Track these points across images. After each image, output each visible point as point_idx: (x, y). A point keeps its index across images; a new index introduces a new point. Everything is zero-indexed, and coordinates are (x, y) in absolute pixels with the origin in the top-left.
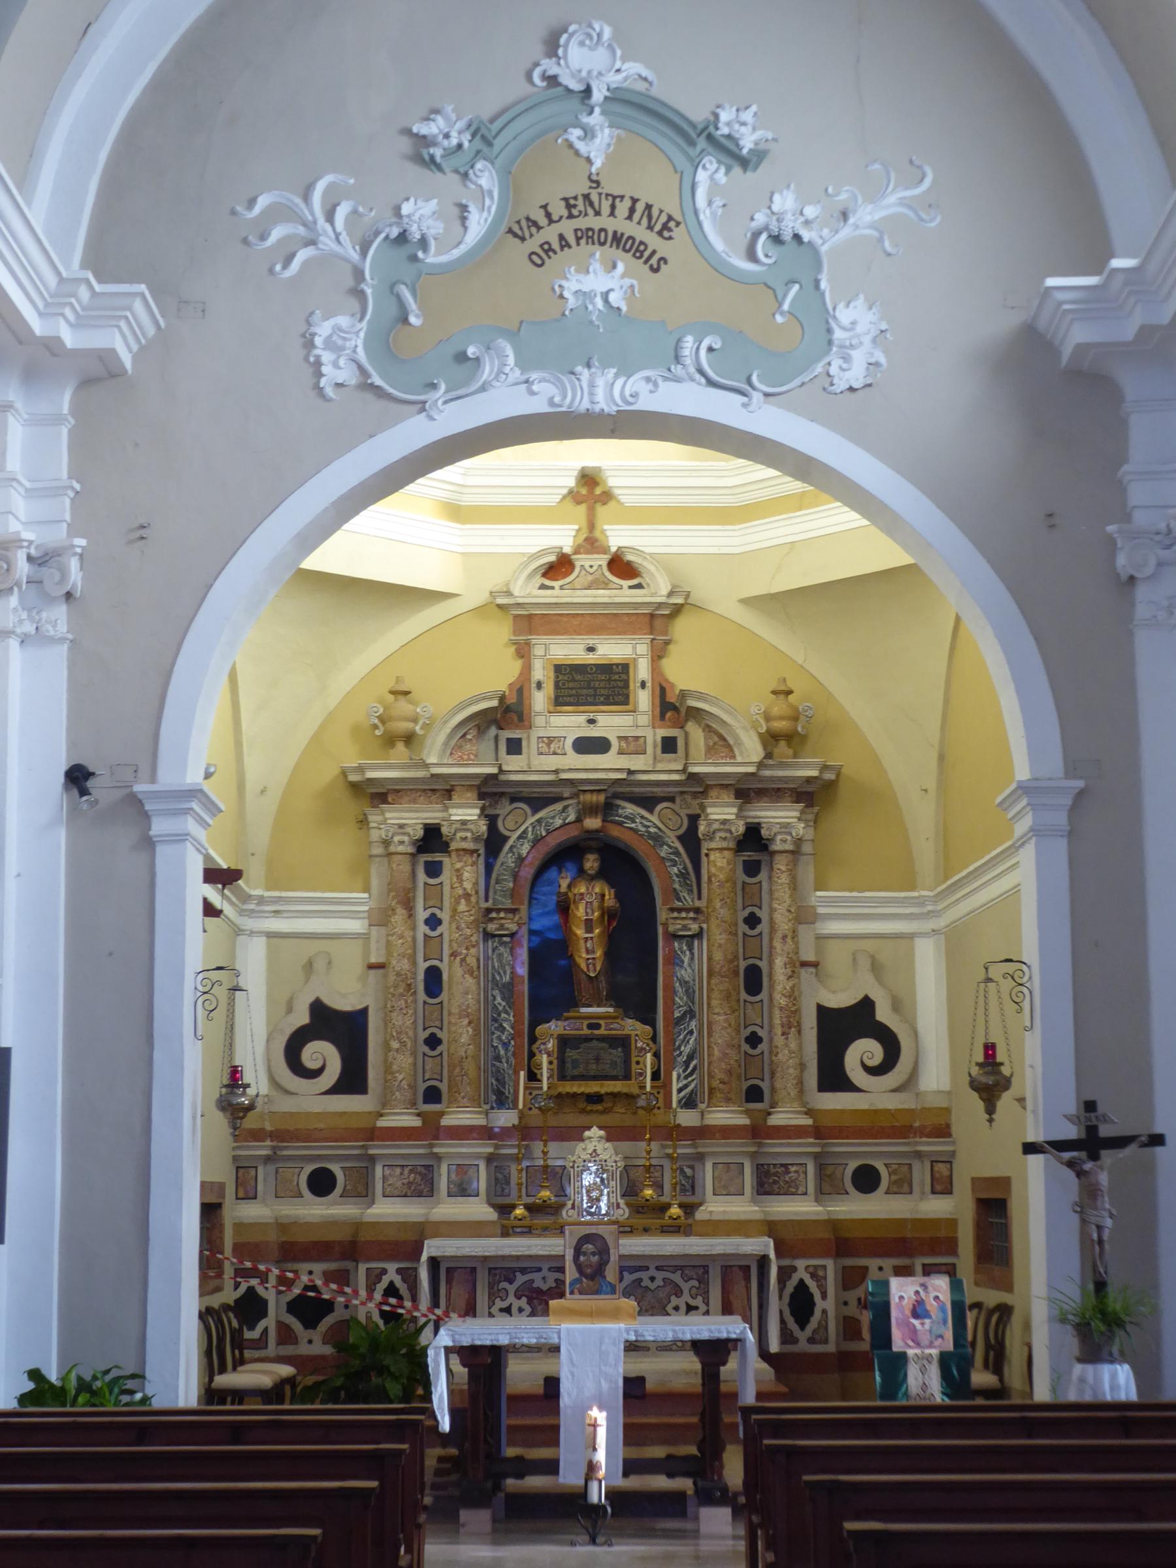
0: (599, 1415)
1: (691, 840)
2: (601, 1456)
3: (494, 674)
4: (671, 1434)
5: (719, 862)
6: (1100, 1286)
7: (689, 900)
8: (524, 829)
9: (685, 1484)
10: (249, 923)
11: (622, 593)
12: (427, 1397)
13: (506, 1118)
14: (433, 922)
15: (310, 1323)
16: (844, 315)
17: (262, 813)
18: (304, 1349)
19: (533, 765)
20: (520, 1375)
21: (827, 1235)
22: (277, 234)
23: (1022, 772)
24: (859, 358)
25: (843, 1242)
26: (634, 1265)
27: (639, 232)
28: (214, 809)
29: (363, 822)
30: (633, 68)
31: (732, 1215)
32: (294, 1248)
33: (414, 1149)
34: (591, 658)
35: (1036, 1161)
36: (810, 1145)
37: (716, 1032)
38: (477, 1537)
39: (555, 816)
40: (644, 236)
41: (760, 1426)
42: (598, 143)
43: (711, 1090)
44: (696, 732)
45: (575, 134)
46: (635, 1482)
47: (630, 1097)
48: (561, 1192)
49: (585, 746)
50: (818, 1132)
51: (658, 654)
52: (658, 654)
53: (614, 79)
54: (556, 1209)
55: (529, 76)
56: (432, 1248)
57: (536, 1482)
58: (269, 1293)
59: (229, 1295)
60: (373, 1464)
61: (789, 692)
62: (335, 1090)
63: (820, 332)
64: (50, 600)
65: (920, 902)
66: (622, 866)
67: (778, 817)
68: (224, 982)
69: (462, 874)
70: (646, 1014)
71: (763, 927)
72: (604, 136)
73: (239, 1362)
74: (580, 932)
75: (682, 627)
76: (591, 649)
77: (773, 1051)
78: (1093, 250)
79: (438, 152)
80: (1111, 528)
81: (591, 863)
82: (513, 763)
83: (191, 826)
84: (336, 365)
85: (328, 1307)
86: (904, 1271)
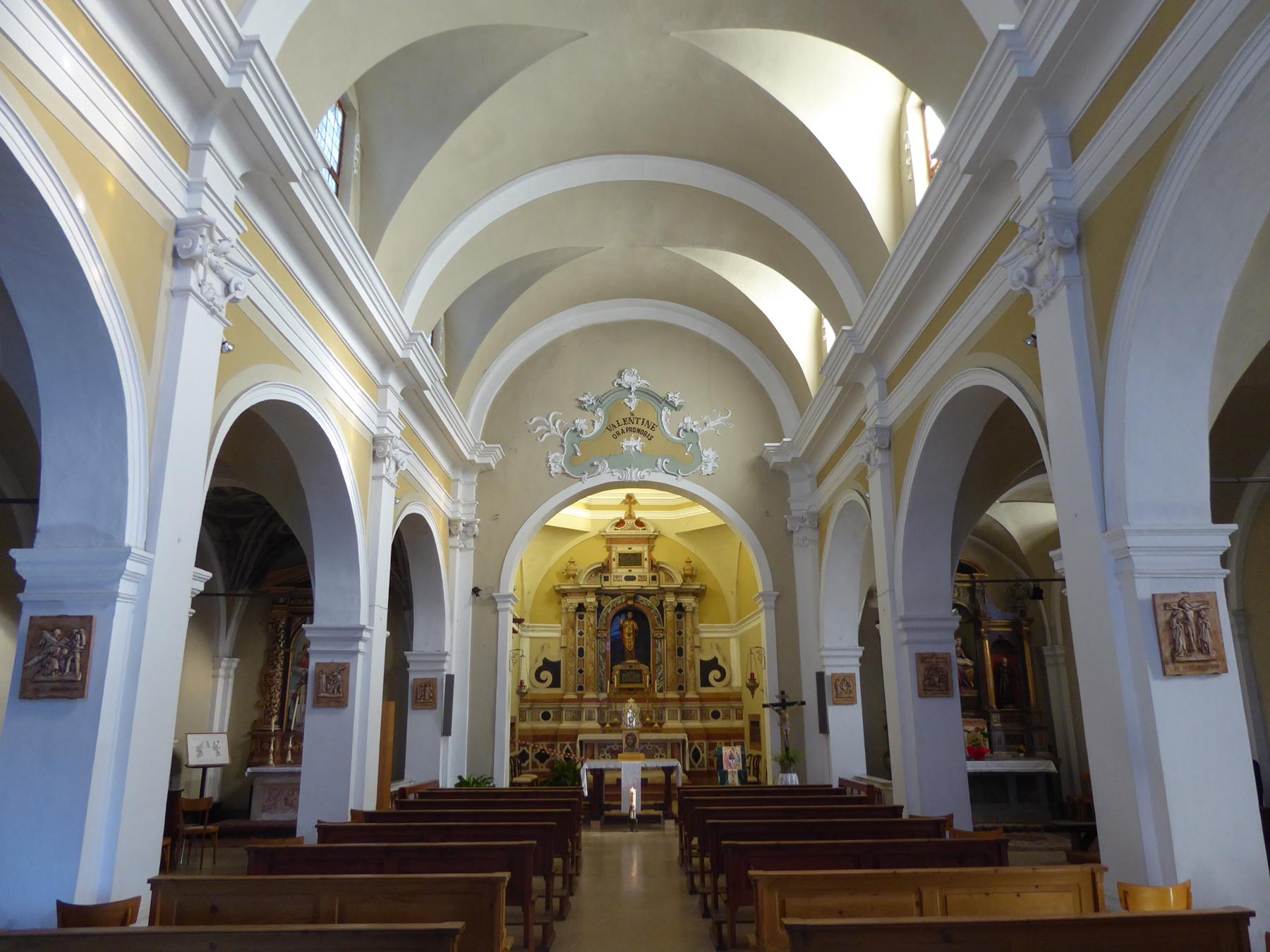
0: (633, 790)
1: (661, 608)
2: (634, 803)
3: (599, 556)
4: (654, 797)
5: (669, 615)
6: (787, 749)
8: (609, 604)
9: (660, 813)
10: (525, 634)
11: (639, 531)
12: (580, 784)
13: (603, 696)
14: (581, 634)
15: (542, 761)
16: (706, 453)
17: (529, 600)
18: (540, 770)
19: (612, 584)
20: (609, 778)
23: (761, 590)
24: (710, 465)
25: (709, 735)
26: (644, 742)
27: (645, 429)
28: (515, 600)
29: (560, 602)
31: (675, 728)
32: (537, 737)
33: (575, 705)
35: (767, 710)
36: (698, 704)
37: (668, 669)
38: (596, 830)
40: (646, 429)
41: (683, 792)
42: (633, 403)
44: (662, 574)
46: (645, 812)
47: (642, 689)
48: (621, 719)
49: (629, 578)
50: (701, 700)
52: (650, 550)
54: (619, 725)
56: (581, 737)
57: (614, 812)
58: (529, 752)
59: (517, 752)
60: (567, 805)
62: (551, 686)
63: (698, 457)
64: (469, 537)
66: (640, 616)
67: (688, 601)
68: (517, 655)
69: (590, 619)
73: (520, 774)
75: (658, 542)
78: (779, 436)
82: (606, 584)
83: (509, 605)
85: (548, 756)
86: (728, 745)
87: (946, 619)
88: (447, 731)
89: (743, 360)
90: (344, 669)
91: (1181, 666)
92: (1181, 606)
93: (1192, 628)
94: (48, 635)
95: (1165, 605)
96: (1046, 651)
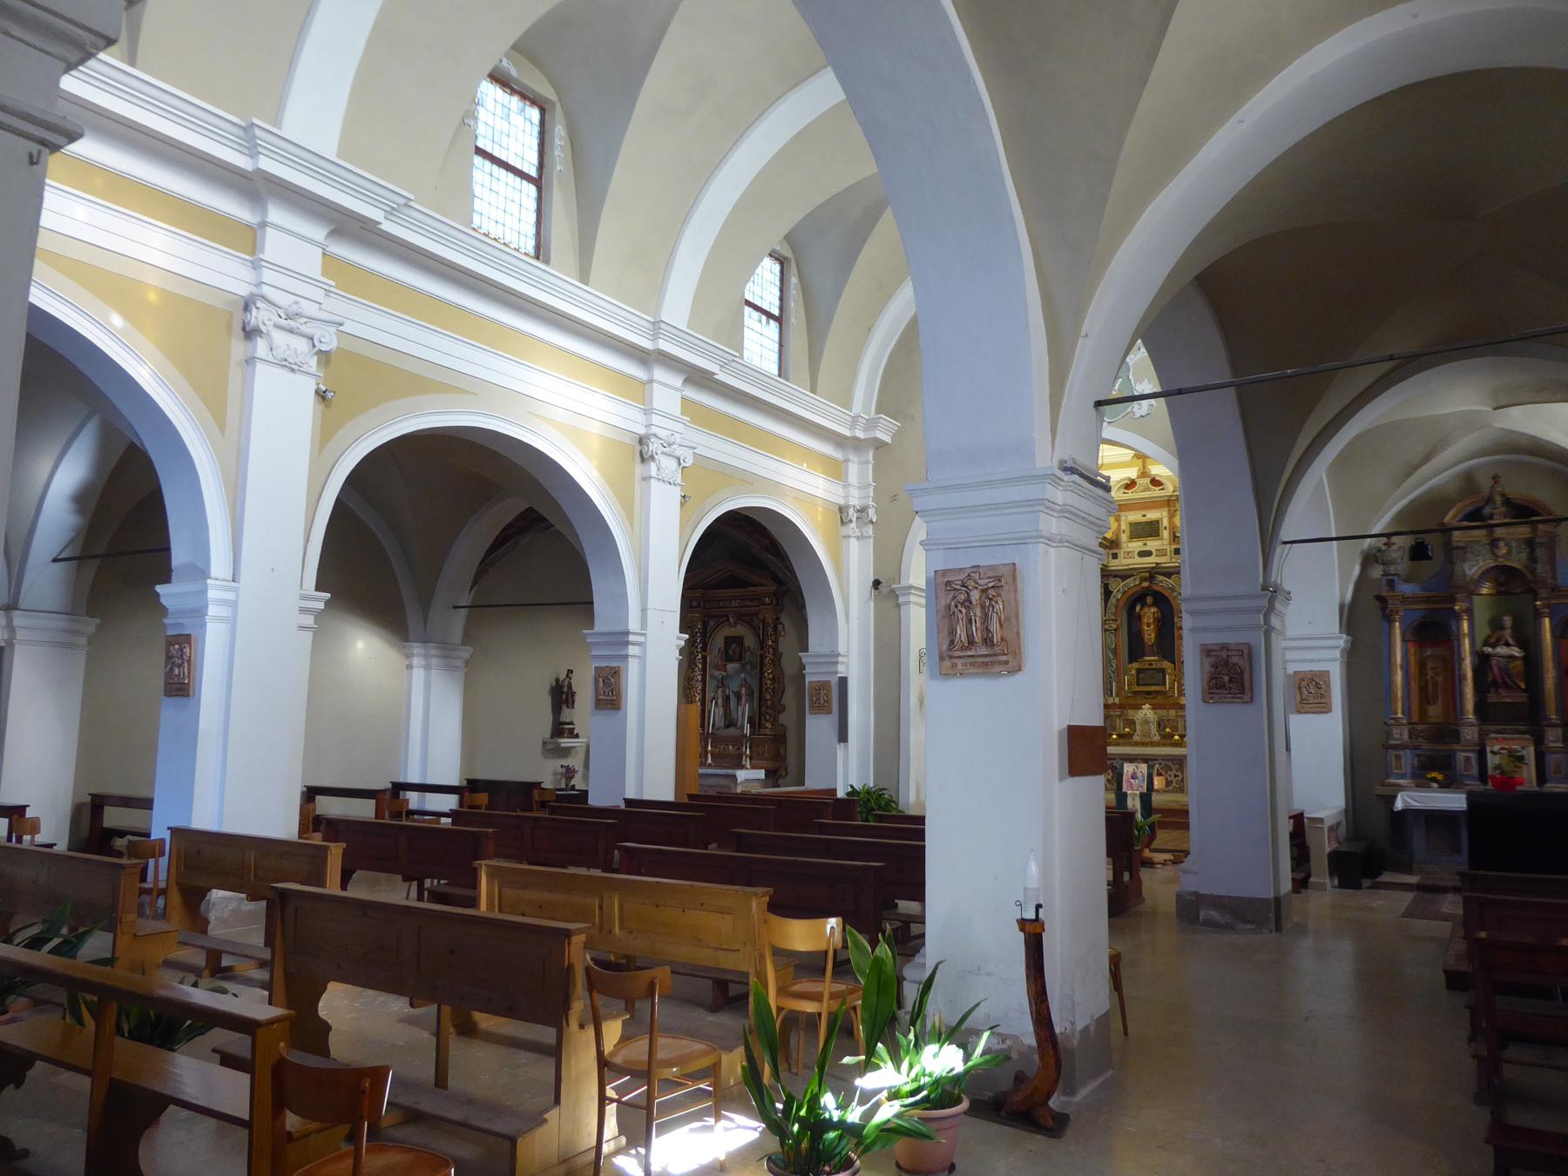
11: (1156, 492)
39: (1131, 582)
47: (1164, 693)
49: (1143, 554)
54: (1130, 736)
81: (1149, 600)
87: (1250, 597)
88: (843, 737)
91: (959, 662)
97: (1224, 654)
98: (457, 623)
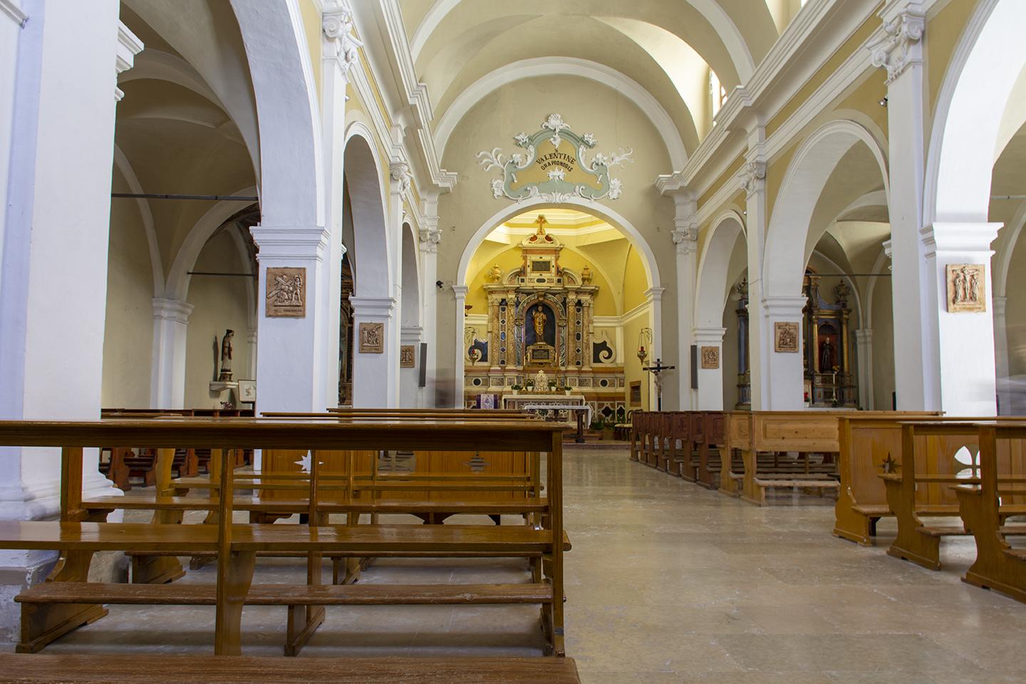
1: (564, 303)
3: (518, 264)
5: (571, 309)
7: (564, 318)
11: (548, 245)
13: (521, 368)
14: (503, 322)
16: (613, 182)
19: (527, 285)
21: (594, 395)
22: (485, 161)
23: (650, 286)
27: (567, 162)
29: (487, 298)
30: (565, 125)
34: (541, 260)
36: (592, 375)
40: (567, 163)
42: (557, 141)
43: (568, 362)
44: (566, 278)
45: (552, 139)
49: (540, 281)
50: (593, 372)
51: (557, 259)
52: (557, 259)
53: (561, 127)
55: (542, 126)
61: (588, 269)
63: (606, 186)
65: (618, 319)
66: (547, 309)
67: (585, 298)
69: (512, 310)
70: (553, 344)
71: (581, 324)
72: (559, 140)
74: (537, 325)
75: (561, 253)
76: (541, 258)
77: (583, 353)
79: (521, 143)
80: (672, 231)
81: (540, 308)
82: (523, 284)
84: (498, 191)
89: (644, 109)
90: (380, 327)
92: (963, 272)
93: (968, 285)
94: (280, 279)
95: (953, 271)
96: (859, 333)
97: (787, 328)
98: (184, 284)
